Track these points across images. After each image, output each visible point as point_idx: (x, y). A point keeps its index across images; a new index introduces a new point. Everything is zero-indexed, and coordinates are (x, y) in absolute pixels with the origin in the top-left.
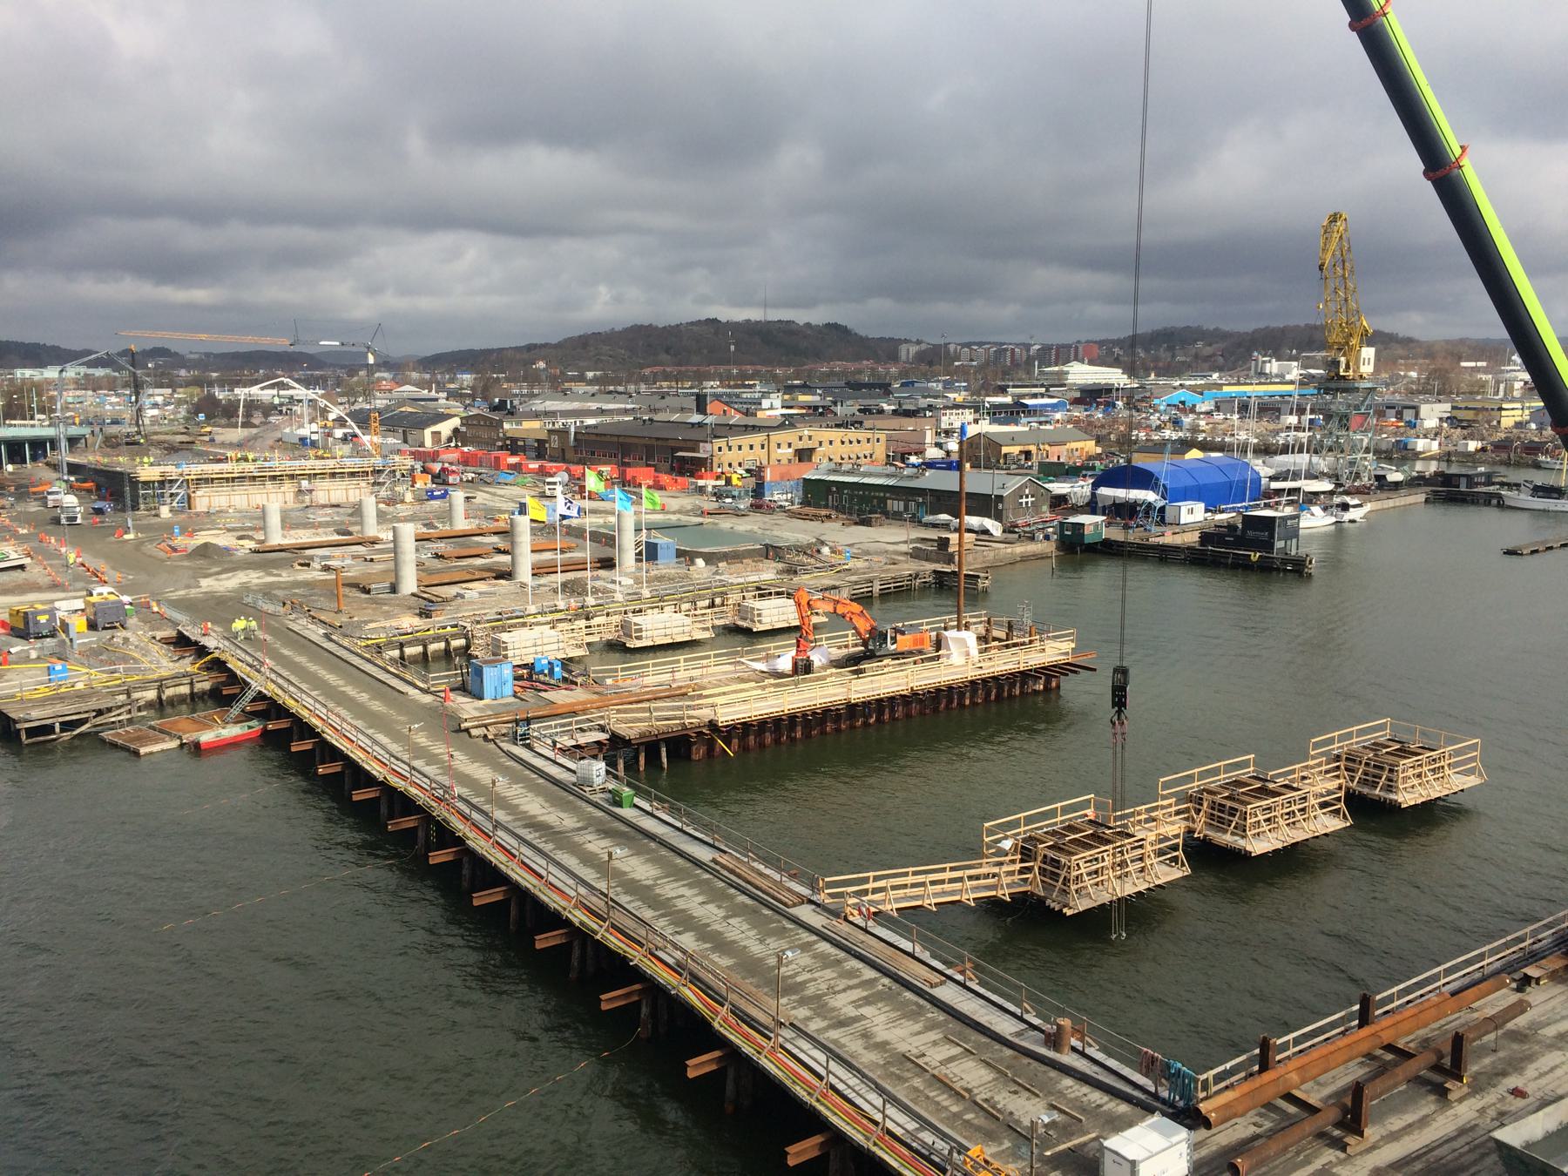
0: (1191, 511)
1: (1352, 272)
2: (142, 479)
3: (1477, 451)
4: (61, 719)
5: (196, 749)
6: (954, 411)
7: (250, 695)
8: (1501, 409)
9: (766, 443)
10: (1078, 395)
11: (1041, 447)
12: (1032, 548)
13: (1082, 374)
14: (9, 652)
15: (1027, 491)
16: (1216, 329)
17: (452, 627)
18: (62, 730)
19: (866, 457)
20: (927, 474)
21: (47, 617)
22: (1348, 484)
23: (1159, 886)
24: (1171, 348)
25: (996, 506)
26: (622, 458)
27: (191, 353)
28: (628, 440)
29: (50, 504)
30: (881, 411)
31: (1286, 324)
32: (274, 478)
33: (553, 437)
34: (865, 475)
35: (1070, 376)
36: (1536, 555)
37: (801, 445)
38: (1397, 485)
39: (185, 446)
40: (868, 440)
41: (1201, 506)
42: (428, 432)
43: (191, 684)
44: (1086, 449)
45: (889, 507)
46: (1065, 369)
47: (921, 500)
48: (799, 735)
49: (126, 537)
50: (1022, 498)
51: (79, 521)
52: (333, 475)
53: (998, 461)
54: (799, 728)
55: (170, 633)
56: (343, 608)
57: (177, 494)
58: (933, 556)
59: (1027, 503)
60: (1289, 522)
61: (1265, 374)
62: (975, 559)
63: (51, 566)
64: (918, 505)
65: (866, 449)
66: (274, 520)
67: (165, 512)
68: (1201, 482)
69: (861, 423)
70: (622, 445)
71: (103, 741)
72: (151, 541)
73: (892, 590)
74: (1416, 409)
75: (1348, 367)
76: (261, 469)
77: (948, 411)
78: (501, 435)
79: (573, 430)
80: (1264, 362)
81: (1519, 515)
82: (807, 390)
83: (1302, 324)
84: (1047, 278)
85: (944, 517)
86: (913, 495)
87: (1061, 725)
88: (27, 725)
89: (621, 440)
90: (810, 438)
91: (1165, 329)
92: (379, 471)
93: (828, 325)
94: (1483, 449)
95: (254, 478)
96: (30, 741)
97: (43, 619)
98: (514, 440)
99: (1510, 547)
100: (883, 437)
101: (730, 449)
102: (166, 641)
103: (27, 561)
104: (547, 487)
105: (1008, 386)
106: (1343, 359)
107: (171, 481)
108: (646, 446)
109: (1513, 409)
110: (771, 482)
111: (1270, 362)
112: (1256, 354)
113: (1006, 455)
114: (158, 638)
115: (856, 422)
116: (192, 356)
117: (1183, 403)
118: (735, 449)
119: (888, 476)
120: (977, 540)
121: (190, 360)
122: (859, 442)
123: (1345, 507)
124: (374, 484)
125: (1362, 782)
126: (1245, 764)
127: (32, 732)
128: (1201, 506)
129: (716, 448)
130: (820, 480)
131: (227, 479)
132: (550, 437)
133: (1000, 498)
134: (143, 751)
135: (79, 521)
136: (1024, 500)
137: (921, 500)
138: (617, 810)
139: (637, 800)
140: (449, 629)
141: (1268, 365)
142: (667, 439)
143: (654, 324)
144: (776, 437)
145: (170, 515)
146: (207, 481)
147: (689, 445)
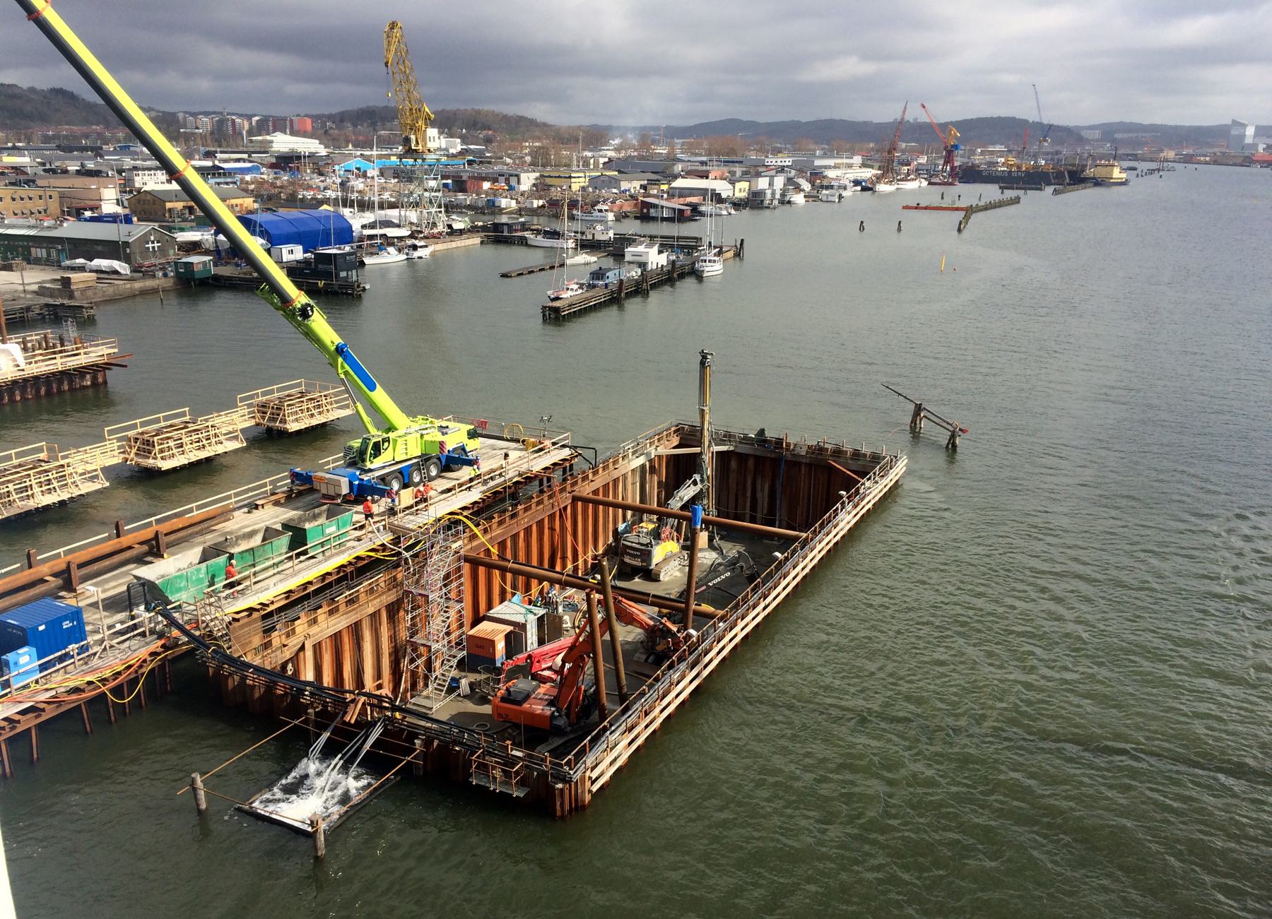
0: (291, 252)
1: (412, 69)
3: (539, 207)
10: (274, 160)
12: (150, 283)
13: (282, 142)
19: (40, 212)
20: (65, 225)
22: (426, 232)
23: (81, 495)
24: (373, 124)
30: (65, 172)
34: (9, 227)
35: (274, 145)
36: (532, 275)
38: (461, 232)
40: (40, 197)
41: (300, 248)
44: (245, 205)
45: (34, 254)
46: (268, 138)
59: (153, 248)
62: (95, 294)
64: (59, 251)
74: (518, 176)
75: (417, 143)
81: (538, 250)
82: (16, 151)
85: (80, 261)
87: (112, 409)
94: (543, 206)
99: (504, 271)
100: (55, 195)
105: (216, 152)
106: (413, 137)
113: (170, 210)
117: (358, 169)
119: (29, 227)
120: (98, 278)
122: (30, 199)
123: (415, 248)
125: (271, 419)
126: (183, 414)
128: (300, 248)
133: (126, 244)
136: (150, 245)
137: (60, 247)
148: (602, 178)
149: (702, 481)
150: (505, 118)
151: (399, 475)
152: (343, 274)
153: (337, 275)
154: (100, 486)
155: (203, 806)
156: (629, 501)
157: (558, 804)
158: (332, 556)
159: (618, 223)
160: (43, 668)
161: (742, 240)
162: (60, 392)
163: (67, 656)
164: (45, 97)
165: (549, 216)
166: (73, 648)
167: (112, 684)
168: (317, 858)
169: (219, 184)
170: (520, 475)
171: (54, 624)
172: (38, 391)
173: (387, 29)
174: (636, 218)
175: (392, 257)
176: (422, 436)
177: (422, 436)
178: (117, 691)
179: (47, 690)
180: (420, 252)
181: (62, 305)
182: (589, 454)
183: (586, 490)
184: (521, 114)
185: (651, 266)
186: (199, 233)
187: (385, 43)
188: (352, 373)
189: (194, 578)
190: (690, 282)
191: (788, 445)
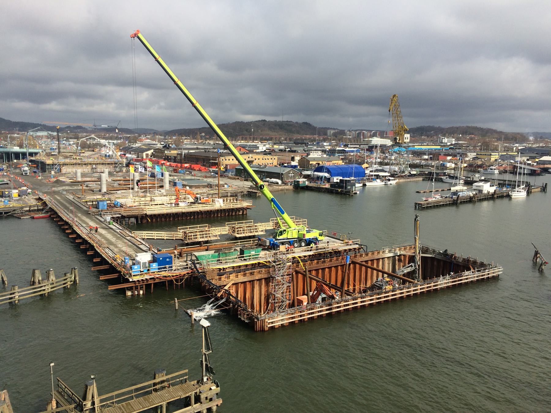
2: (47, 163)
5: (33, 218)
6: (315, 151)
7: (48, 208)
8: (491, 155)
11: (323, 162)
15: (291, 172)
16: (439, 127)
18: (5, 214)
19: (270, 164)
27: (89, 128)
28: (198, 157)
29: (22, 170)
31: (452, 126)
32: (85, 164)
35: (372, 142)
36: (418, 193)
37: (249, 160)
38: (414, 175)
40: (271, 159)
42: (144, 154)
43: (38, 207)
48: (171, 219)
49: (39, 178)
50: (289, 174)
51: (28, 174)
52: (103, 164)
54: (172, 218)
55: (37, 197)
56: (84, 194)
57: (57, 168)
58: (255, 188)
59: (291, 176)
60: (352, 182)
61: (443, 143)
63: (15, 184)
64: (263, 176)
65: (271, 161)
66: (79, 175)
67: (53, 172)
68: (344, 172)
69: (271, 154)
71: (14, 216)
72: (45, 179)
77: (313, 152)
78: (164, 155)
79: (183, 154)
80: (442, 139)
86: (262, 173)
89: (196, 157)
90: (252, 157)
92: (116, 163)
94: (467, 167)
95: (79, 164)
97: (7, 193)
98: (168, 156)
101: (226, 160)
103: (9, 182)
105: (348, 145)
107: (55, 164)
108: (203, 159)
109: (495, 155)
110: (229, 169)
111: (444, 138)
113: (311, 164)
116: (89, 129)
118: (227, 160)
122: (268, 159)
123: (389, 180)
124: (114, 167)
129: (221, 160)
131: (72, 164)
133: (282, 174)
134: (22, 218)
135: (28, 174)
136: (290, 175)
138: (109, 225)
139: (114, 224)
141: (444, 140)
143: (243, 121)
147: (214, 158)
148: (506, 156)
149: (415, 266)
150: (481, 129)
151: (289, 243)
152: (349, 187)
153: (346, 188)
154: (217, 239)
155: (177, 308)
156: (386, 270)
157: (255, 326)
158: (251, 260)
159: (500, 175)
160: (159, 269)
161: (546, 184)
162: (232, 215)
163: (165, 268)
164: (300, 125)
165: (468, 171)
166: (167, 266)
167: (175, 277)
168: (192, 324)
169: (339, 156)
170: (333, 250)
171: (164, 259)
172: (225, 214)
173: (392, 97)
174: (511, 173)
175: (378, 183)
176: (299, 231)
177: (299, 231)
178: (177, 280)
179: (158, 275)
180: (391, 182)
181: (252, 191)
182: (365, 248)
183: (359, 260)
184: (490, 128)
185: (485, 192)
186: (310, 172)
187: (390, 102)
188: (276, 208)
189: (208, 257)
190: (506, 200)
191: (455, 257)
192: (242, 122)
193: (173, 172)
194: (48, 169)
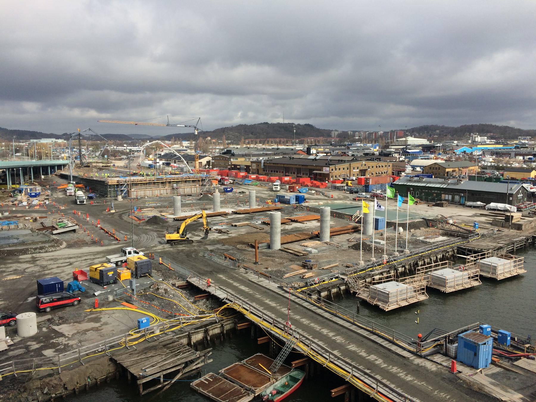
2: (110, 184)
4: (165, 373)
9: (349, 167)
14: (94, 294)
17: (336, 278)
21: (112, 273)
25: (509, 199)
26: (285, 173)
28: (288, 166)
29: (68, 194)
33: (253, 164)
37: (362, 168)
39: (104, 168)
40: (386, 166)
47: (462, 195)
51: (85, 203)
52: (186, 181)
53: (444, 175)
57: (124, 190)
64: (461, 197)
65: (384, 170)
70: (285, 168)
73: (519, 247)
76: (158, 179)
78: (230, 163)
79: (263, 161)
80: (475, 137)
83: (478, 124)
84: (391, 109)
88: (144, 381)
89: (285, 166)
91: (424, 126)
93: (306, 125)
95: (154, 183)
96: (145, 392)
97: (110, 274)
102: (181, 287)
103: (76, 227)
104: (274, 187)
110: (372, 185)
112: (472, 134)
113: (448, 172)
114: (177, 285)
115: (377, 159)
116: (87, 136)
121: (86, 137)
124: (202, 185)
127: (147, 385)
130: (403, 185)
132: (252, 165)
133: (511, 195)
135: (85, 203)
140: (334, 279)
141: (477, 138)
142: (307, 166)
143: (242, 124)
144: (354, 164)
145: (122, 200)
146: (136, 184)
147: (317, 168)
192: (245, 125)
193: (289, 191)
194: (358, 254)
